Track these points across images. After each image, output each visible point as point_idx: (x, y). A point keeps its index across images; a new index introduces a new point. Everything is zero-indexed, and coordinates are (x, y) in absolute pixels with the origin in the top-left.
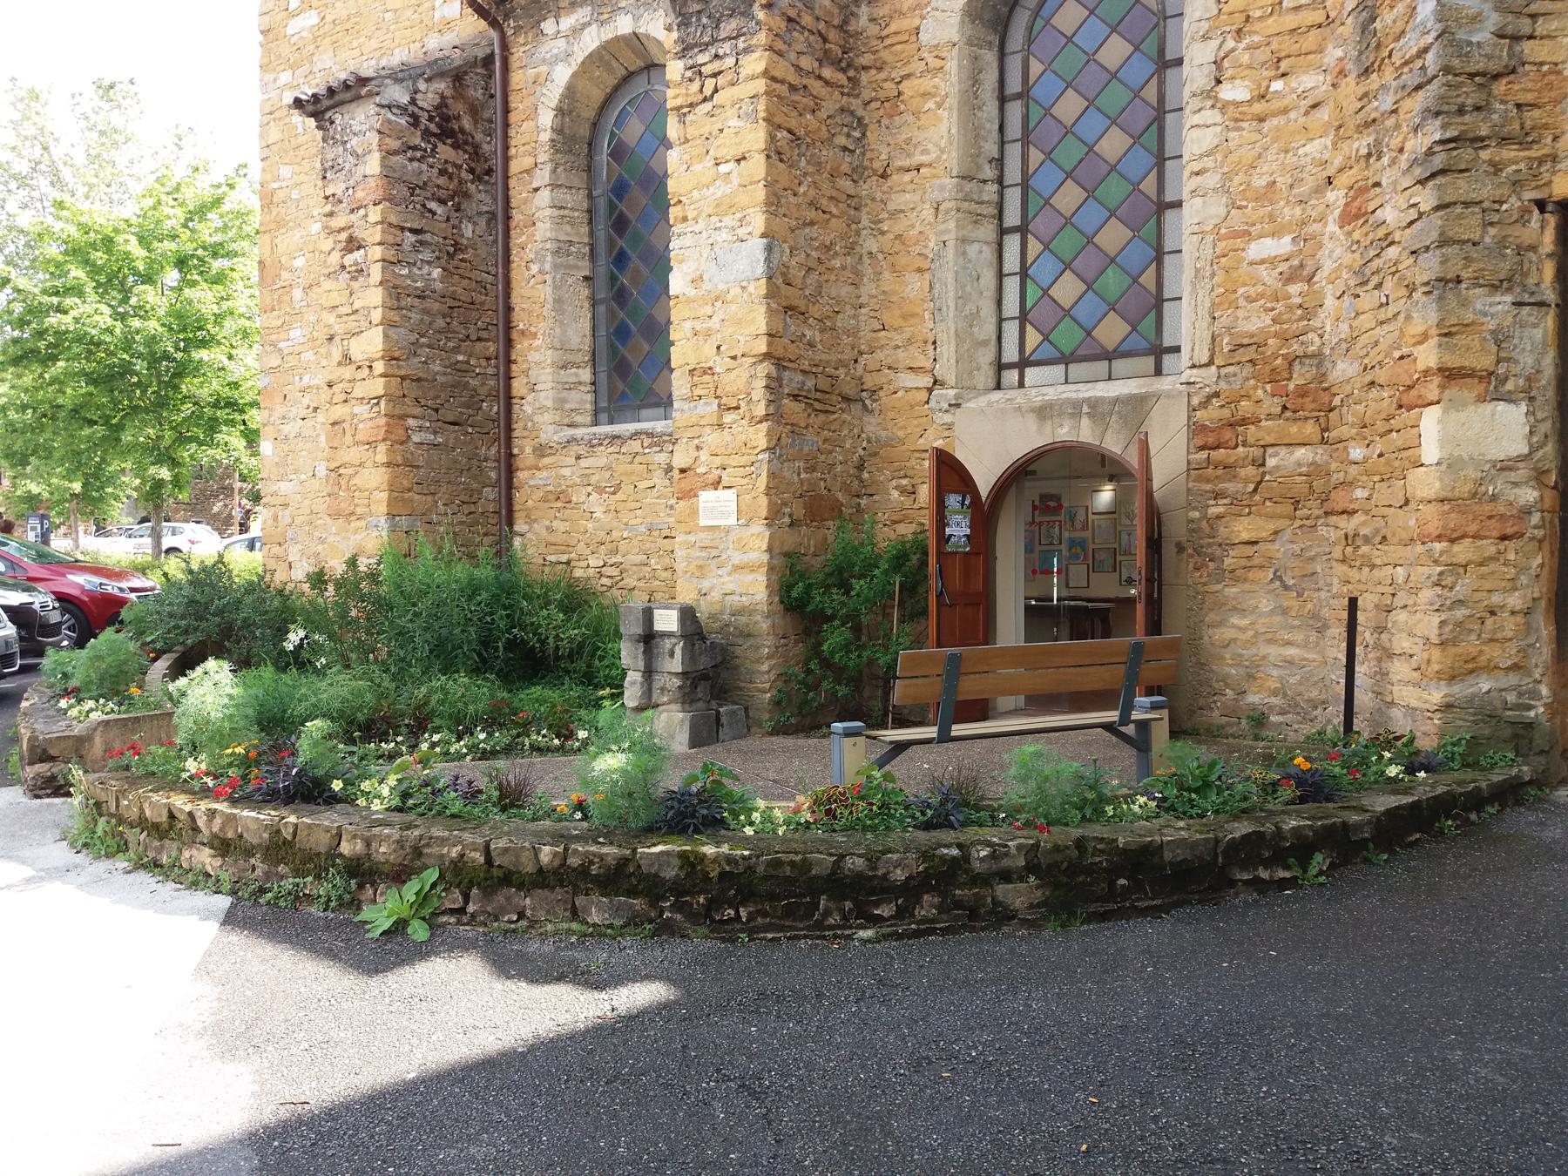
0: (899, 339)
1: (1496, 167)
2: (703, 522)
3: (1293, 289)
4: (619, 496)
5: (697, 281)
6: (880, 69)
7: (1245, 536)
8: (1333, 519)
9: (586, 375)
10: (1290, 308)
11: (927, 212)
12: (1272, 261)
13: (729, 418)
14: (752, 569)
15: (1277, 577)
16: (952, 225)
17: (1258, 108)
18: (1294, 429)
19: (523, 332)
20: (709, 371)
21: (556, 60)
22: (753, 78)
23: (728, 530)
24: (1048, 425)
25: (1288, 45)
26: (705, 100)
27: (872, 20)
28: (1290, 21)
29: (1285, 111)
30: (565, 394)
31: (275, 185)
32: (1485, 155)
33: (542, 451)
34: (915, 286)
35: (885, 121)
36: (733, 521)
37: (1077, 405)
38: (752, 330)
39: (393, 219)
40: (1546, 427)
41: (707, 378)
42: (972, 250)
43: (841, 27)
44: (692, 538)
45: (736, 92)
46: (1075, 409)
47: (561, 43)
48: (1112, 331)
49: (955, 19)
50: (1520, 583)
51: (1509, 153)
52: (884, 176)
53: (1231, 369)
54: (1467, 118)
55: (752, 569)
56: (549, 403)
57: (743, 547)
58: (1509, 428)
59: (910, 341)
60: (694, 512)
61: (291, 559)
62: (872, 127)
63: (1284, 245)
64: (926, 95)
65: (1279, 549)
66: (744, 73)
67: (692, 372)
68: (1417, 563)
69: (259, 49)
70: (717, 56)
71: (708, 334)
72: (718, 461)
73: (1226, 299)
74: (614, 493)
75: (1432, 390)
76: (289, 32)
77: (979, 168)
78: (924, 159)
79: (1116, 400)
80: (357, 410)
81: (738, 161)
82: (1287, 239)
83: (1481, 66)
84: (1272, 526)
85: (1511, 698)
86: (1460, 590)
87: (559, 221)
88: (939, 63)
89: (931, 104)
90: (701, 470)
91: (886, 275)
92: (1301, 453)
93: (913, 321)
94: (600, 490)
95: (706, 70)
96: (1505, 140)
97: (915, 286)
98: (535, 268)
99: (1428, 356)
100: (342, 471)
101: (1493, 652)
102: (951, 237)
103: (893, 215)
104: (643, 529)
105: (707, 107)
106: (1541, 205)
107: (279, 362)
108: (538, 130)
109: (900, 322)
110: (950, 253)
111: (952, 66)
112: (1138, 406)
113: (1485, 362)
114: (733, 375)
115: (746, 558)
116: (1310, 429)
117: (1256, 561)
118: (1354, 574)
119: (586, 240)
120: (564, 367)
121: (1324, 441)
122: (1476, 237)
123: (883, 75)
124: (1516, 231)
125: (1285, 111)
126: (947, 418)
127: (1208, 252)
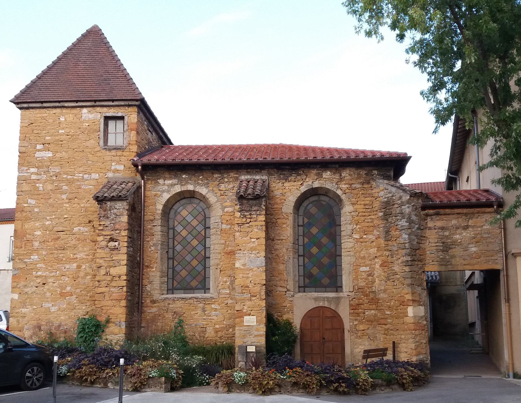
0: (277, 279)
1: (418, 265)
2: (245, 324)
3: (370, 278)
5: (244, 265)
6: (271, 215)
7: (362, 329)
10: (369, 282)
11: (284, 250)
12: (365, 272)
13: (253, 298)
14: (261, 336)
15: (369, 338)
16: (291, 254)
18: (371, 306)
19: (147, 266)
20: (248, 287)
21: (163, 191)
22: (261, 221)
24: (317, 302)
25: (367, 229)
28: (367, 224)
29: (366, 242)
32: (416, 263)
33: (154, 302)
34: (282, 267)
36: (255, 324)
37: (324, 298)
38: (261, 278)
44: (241, 328)
45: (256, 223)
46: (324, 299)
47: (166, 187)
48: (326, 281)
49: (292, 208)
50: (424, 338)
56: (158, 288)
57: (257, 330)
58: (421, 311)
59: (281, 280)
63: (368, 269)
64: (284, 224)
65: (369, 332)
68: (408, 334)
69: (18, 158)
70: (251, 214)
71: (248, 278)
72: (250, 309)
73: (356, 279)
75: (411, 303)
76: (36, 155)
79: (333, 298)
82: (368, 268)
84: (368, 326)
86: (417, 340)
88: (287, 217)
89: (285, 226)
90: (245, 311)
91: (274, 264)
96: (419, 261)
97: (282, 267)
98: (153, 248)
99: (409, 297)
100: (103, 308)
102: (291, 257)
105: (248, 225)
107: (25, 266)
110: (291, 261)
115: (259, 333)
116: (374, 306)
117: (365, 334)
120: (162, 277)
121: (377, 309)
123: (272, 217)
124: (420, 276)
125: (366, 242)
126: (291, 299)
127: (352, 268)
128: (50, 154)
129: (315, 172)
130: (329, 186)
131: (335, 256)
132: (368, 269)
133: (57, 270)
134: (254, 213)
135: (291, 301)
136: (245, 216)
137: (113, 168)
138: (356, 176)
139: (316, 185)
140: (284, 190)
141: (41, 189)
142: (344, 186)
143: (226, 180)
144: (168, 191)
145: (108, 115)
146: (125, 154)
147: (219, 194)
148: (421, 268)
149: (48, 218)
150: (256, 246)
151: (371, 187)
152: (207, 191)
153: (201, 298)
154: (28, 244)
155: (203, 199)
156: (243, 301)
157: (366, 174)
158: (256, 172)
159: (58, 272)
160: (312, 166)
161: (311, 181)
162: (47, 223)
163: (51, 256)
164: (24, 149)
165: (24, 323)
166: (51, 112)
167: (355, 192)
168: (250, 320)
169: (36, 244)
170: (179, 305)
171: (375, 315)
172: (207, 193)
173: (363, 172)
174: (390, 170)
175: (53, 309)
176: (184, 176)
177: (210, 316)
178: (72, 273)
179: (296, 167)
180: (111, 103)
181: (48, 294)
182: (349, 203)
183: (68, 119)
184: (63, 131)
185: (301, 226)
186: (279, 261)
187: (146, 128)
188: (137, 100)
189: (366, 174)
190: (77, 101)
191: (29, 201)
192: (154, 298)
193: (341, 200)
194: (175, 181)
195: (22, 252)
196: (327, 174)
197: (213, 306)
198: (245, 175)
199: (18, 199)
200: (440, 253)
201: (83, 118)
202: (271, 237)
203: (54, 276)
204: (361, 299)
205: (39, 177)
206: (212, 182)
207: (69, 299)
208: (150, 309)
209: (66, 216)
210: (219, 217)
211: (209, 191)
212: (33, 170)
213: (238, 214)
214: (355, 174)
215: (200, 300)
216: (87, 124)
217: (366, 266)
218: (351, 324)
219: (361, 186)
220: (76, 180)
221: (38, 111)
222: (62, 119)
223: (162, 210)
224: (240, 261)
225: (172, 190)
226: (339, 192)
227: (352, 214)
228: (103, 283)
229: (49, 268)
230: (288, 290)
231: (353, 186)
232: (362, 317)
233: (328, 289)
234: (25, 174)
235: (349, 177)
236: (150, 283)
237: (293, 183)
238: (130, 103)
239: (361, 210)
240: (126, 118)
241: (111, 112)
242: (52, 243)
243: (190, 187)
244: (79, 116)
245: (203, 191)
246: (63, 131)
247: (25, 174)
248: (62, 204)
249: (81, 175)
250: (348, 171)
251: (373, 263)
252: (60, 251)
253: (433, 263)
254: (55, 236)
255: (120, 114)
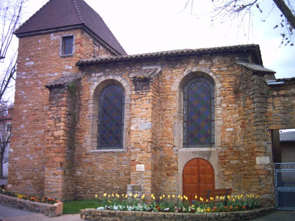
2: (137, 170)
3: (233, 136)
4: (106, 164)
5: (137, 128)
6: (163, 93)
7: (228, 174)
8: (241, 172)
9: (96, 139)
11: (172, 118)
12: (230, 132)
13: (143, 152)
14: (148, 178)
17: (228, 108)
18: (234, 157)
21: (95, 81)
23: (142, 172)
26: (140, 98)
27: (162, 85)
30: (92, 143)
31: (19, 95)
32: (263, 123)
33: (87, 154)
35: (165, 102)
36: (144, 170)
39: (66, 110)
40: (272, 160)
41: (138, 145)
42: (180, 124)
43: (158, 87)
44: (135, 173)
47: (96, 78)
51: (265, 123)
52: (164, 111)
53: (224, 148)
54: (260, 118)
55: (148, 178)
57: (146, 174)
60: (135, 168)
61: (17, 175)
62: (162, 102)
63: (232, 129)
66: (148, 95)
67: (135, 143)
72: (140, 159)
73: (223, 136)
74: (104, 163)
77: (181, 111)
78: (172, 109)
80: (55, 145)
81: (146, 109)
82: (232, 129)
83: (262, 112)
85: (270, 197)
87: (94, 110)
90: (137, 161)
91: (164, 127)
92: (235, 161)
93: (169, 135)
94: (101, 162)
95: (141, 93)
96: (265, 121)
100: (50, 158)
101: (267, 191)
103: (166, 117)
104: (111, 170)
105: (140, 100)
106: (269, 130)
108: (90, 93)
109: (167, 135)
111: (177, 94)
112: (209, 154)
113: (264, 151)
114: (144, 144)
115: (146, 177)
117: (230, 178)
118: (245, 180)
119: (98, 114)
120: (92, 138)
121: (239, 159)
122: (262, 134)
124: (266, 133)
128: (32, 63)
129: (193, 61)
130: (203, 70)
131: (210, 121)
132: (232, 129)
133: (34, 133)
134: (144, 91)
135: (177, 154)
136: (138, 93)
137: (66, 68)
138: (223, 62)
139: (195, 70)
140: (172, 75)
141: (28, 84)
142: (214, 70)
143: (133, 71)
144: (97, 81)
145: (64, 36)
146: (73, 59)
147: (129, 81)
148: (267, 127)
149: (31, 102)
150: (145, 114)
151: (234, 69)
152: (121, 79)
153: (116, 152)
154: (20, 118)
155: (119, 84)
156: (135, 153)
157: (230, 60)
158: (153, 64)
159: (34, 135)
160: (190, 57)
161: (192, 68)
162: (30, 105)
163: (31, 125)
164: (19, 61)
165: (16, 166)
166: (35, 38)
167: (223, 73)
168: (140, 167)
169: (24, 118)
170: (102, 157)
171: (238, 164)
172: (121, 81)
173: (228, 59)
174: (248, 56)
175: (31, 158)
176: (107, 70)
177: (122, 164)
178: (41, 135)
179: (179, 58)
180: (66, 28)
181: (28, 149)
182: (218, 82)
183: (43, 41)
184: (40, 48)
185: (186, 100)
186: (168, 125)
187: (92, 43)
188: (80, 25)
189: (230, 60)
190: (47, 29)
191: (22, 92)
192: (87, 152)
193: (213, 80)
194: (102, 74)
195: (16, 123)
196: (202, 62)
197: (124, 158)
198: (145, 66)
199: (16, 91)
200: (282, 115)
201: (51, 39)
202: (163, 109)
203: (32, 138)
204: (227, 152)
205: (27, 77)
206: (124, 73)
207: (40, 152)
208: (85, 159)
209: (40, 100)
210: (129, 96)
211: (122, 79)
212: (24, 73)
213: (134, 92)
214: (222, 60)
215: (116, 154)
216: (53, 43)
217: (231, 127)
218: (220, 170)
219: (226, 69)
220: (45, 77)
221: (27, 38)
222: (40, 41)
223: (94, 93)
224: (134, 125)
225: (99, 80)
226: (211, 74)
227: (221, 89)
228: (50, 142)
229: (30, 133)
230: (174, 146)
231: (221, 69)
232: (228, 165)
233: (204, 145)
234: (20, 76)
235: (218, 63)
236: (85, 142)
237: (178, 70)
238: (76, 27)
239: (227, 86)
240: (74, 37)
241: (66, 34)
242: (32, 117)
243: (111, 77)
244: (48, 38)
245: (119, 79)
246: (40, 48)
247: (20, 76)
248: (38, 93)
249: (48, 74)
250: (217, 59)
251: (235, 125)
252: (36, 122)
253: (276, 123)
254: (33, 113)
255: (71, 35)
